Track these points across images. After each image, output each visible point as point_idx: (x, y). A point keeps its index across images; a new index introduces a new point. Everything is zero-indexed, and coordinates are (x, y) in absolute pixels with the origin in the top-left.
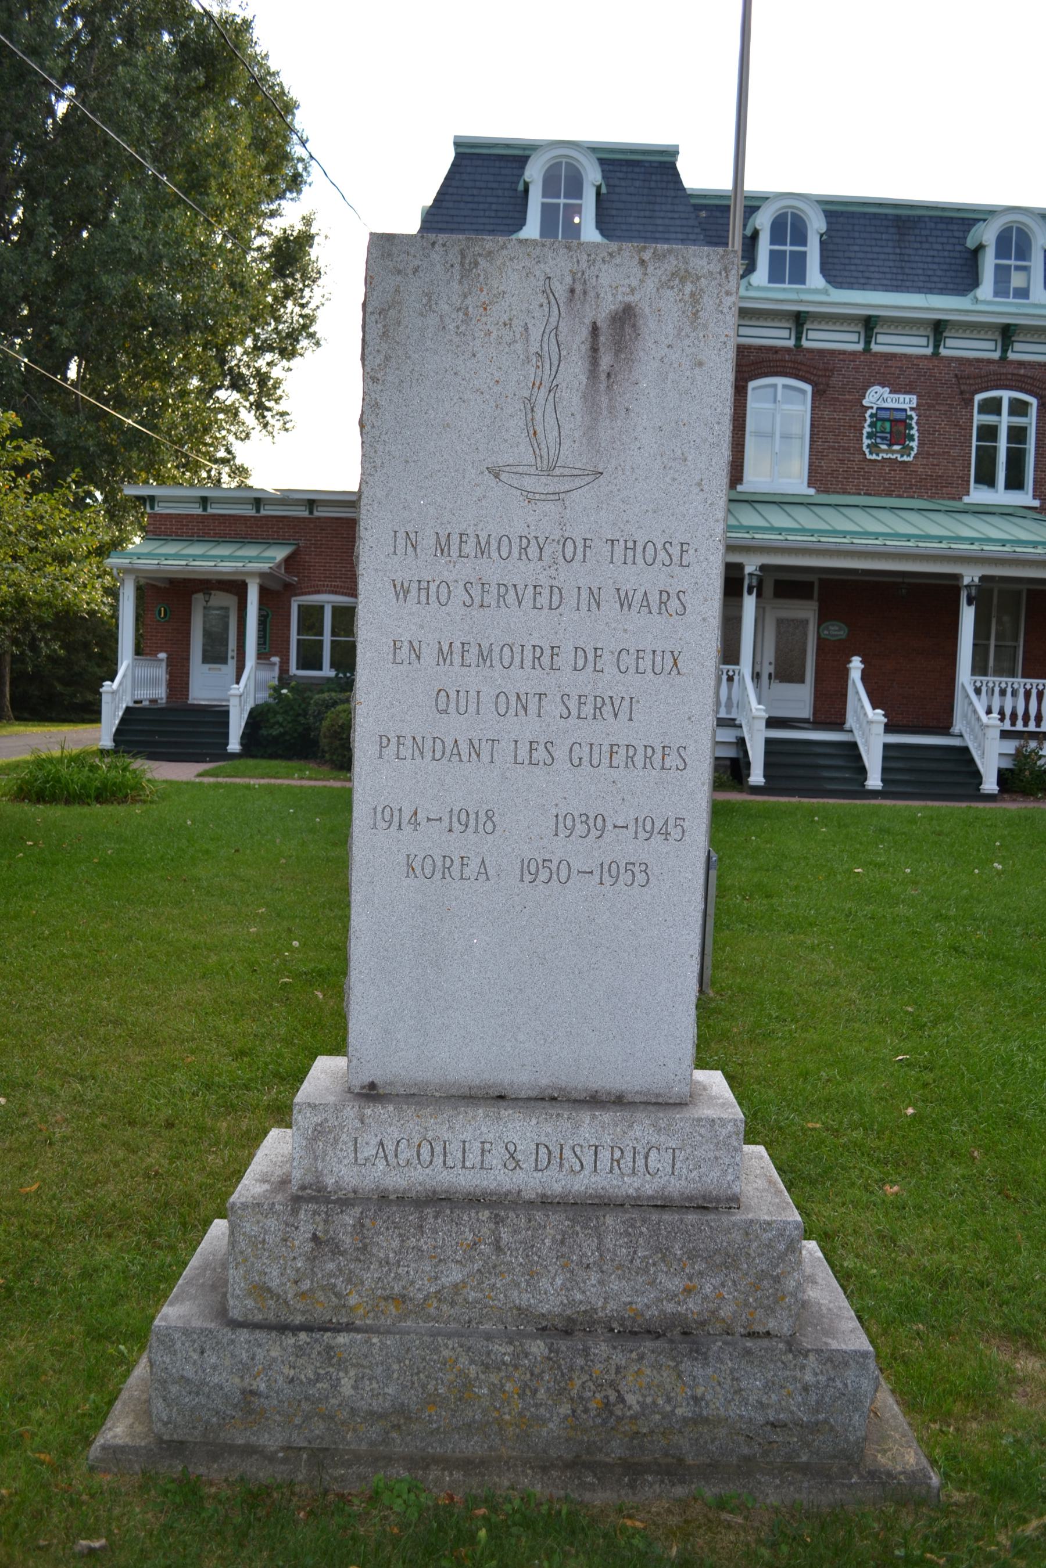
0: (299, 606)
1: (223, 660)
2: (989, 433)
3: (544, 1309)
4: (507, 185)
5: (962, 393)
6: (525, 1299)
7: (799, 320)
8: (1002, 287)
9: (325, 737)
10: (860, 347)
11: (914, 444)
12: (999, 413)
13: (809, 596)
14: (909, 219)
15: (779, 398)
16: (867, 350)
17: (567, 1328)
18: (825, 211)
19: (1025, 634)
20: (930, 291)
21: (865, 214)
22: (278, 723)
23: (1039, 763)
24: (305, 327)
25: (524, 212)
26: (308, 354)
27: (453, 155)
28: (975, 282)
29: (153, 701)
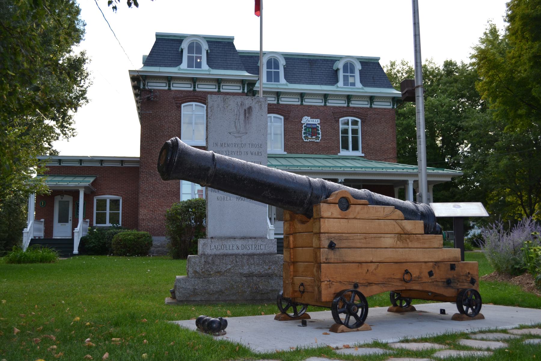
0: (97, 200)
1: (67, 221)
2: (345, 131)
3: (245, 272)
4: (175, 49)
6: (241, 271)
7: (278, 94)
8: (346, 82)
9: (114, 244)
10: (299, 103)
11: (320, 136)
12: (348, 125)
14: (313, 60)
15: (272, 121)
16: (302, 104)
17: (250, 275)
18: (285, 58)
20: (322, 84)
21: (298, 58)
22: (93, 242)
24: (82, 95)
25: (182, 59)
26: (83, 106)
27: (155, 40)
28: (337, 81)
29: (39, 237)
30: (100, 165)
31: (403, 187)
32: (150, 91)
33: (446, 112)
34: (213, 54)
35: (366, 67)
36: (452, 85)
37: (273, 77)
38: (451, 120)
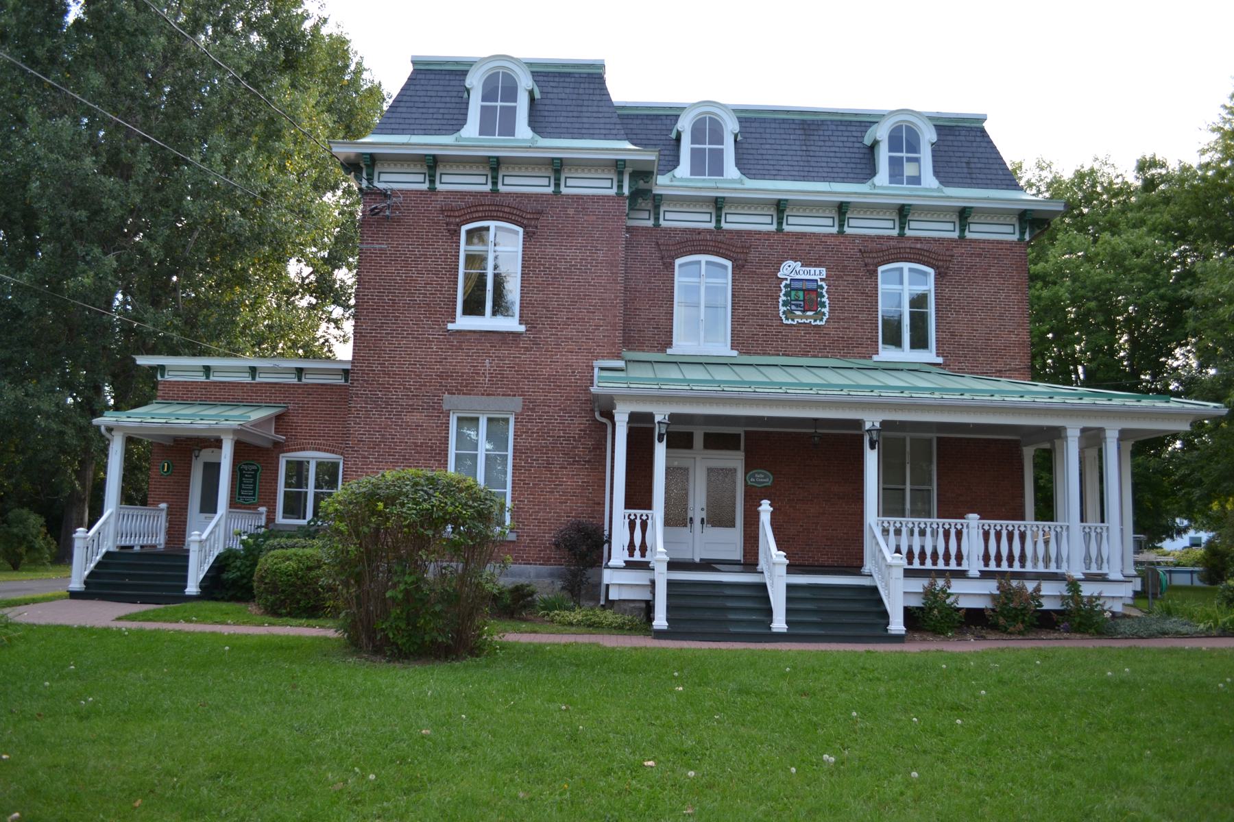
0: (288, 462)
4: (455, 94)
5: (866, 265)
7: (718, 205)
11: (826, 310)
13: (737, 448)
15: (703, 272)
16: (780, 230)
19: (938, 479)
20: (834, 180)
23: (948, 601)
28: (872, 172)
30: (295, 381)
31: (1047, 446)
32: (384, 194)
33: (1145, 269)
34: (548, 102)
35: (950, 138)
36: (1156, 209)
37: (708, 163)
38: (1158, 287)
